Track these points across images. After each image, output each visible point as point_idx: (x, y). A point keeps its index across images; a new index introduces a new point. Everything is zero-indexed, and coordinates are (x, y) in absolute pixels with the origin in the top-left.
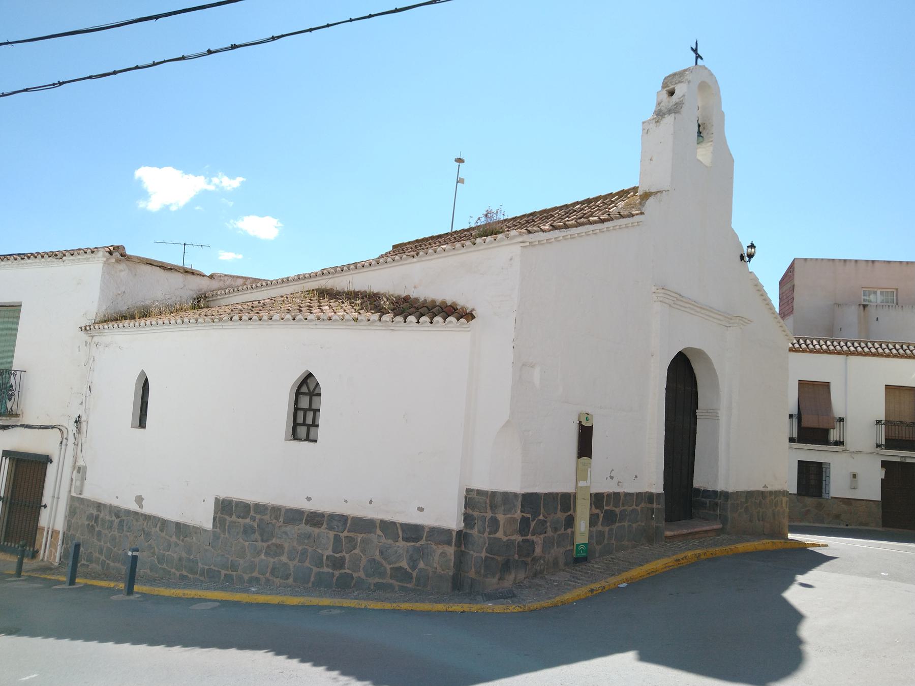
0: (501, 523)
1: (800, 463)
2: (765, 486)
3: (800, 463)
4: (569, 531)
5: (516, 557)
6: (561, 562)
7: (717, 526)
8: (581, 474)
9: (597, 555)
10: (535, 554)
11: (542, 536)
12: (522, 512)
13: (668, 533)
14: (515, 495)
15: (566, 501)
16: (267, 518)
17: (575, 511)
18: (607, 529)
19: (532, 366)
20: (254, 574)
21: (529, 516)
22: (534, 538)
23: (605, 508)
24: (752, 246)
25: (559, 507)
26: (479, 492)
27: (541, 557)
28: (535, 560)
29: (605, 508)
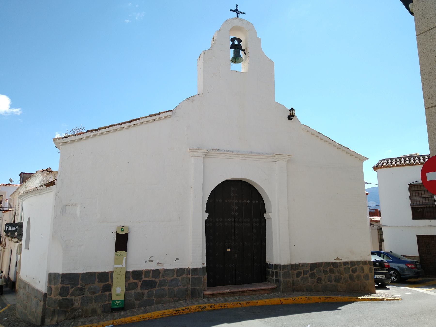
0: (53, 289)
1: (418, 237)
2: (338, 259)
3: (418, 237)
4: (107, 293)
5: (58, 308)
6: (99, 311)
7: (274, 286)
8: (118, 261)
9: (137, 306)
10: (74, 306)
11: (81, 297)
12: (61, 283)
13: (207, 293)
14: (59, 274)
15: (105, 278)
16: (332, 267)
17: (112, 281)
18: (146, 291)
19: (75, 205)
20: (136, 302)
21: (69, 286)
22: (73, 298)
23: (144, 279)
24: (292, 110)
25: (97, 280)
26: (55, 274)
27: (79, 308)
28: (75, 310)
29: (144, 279)
